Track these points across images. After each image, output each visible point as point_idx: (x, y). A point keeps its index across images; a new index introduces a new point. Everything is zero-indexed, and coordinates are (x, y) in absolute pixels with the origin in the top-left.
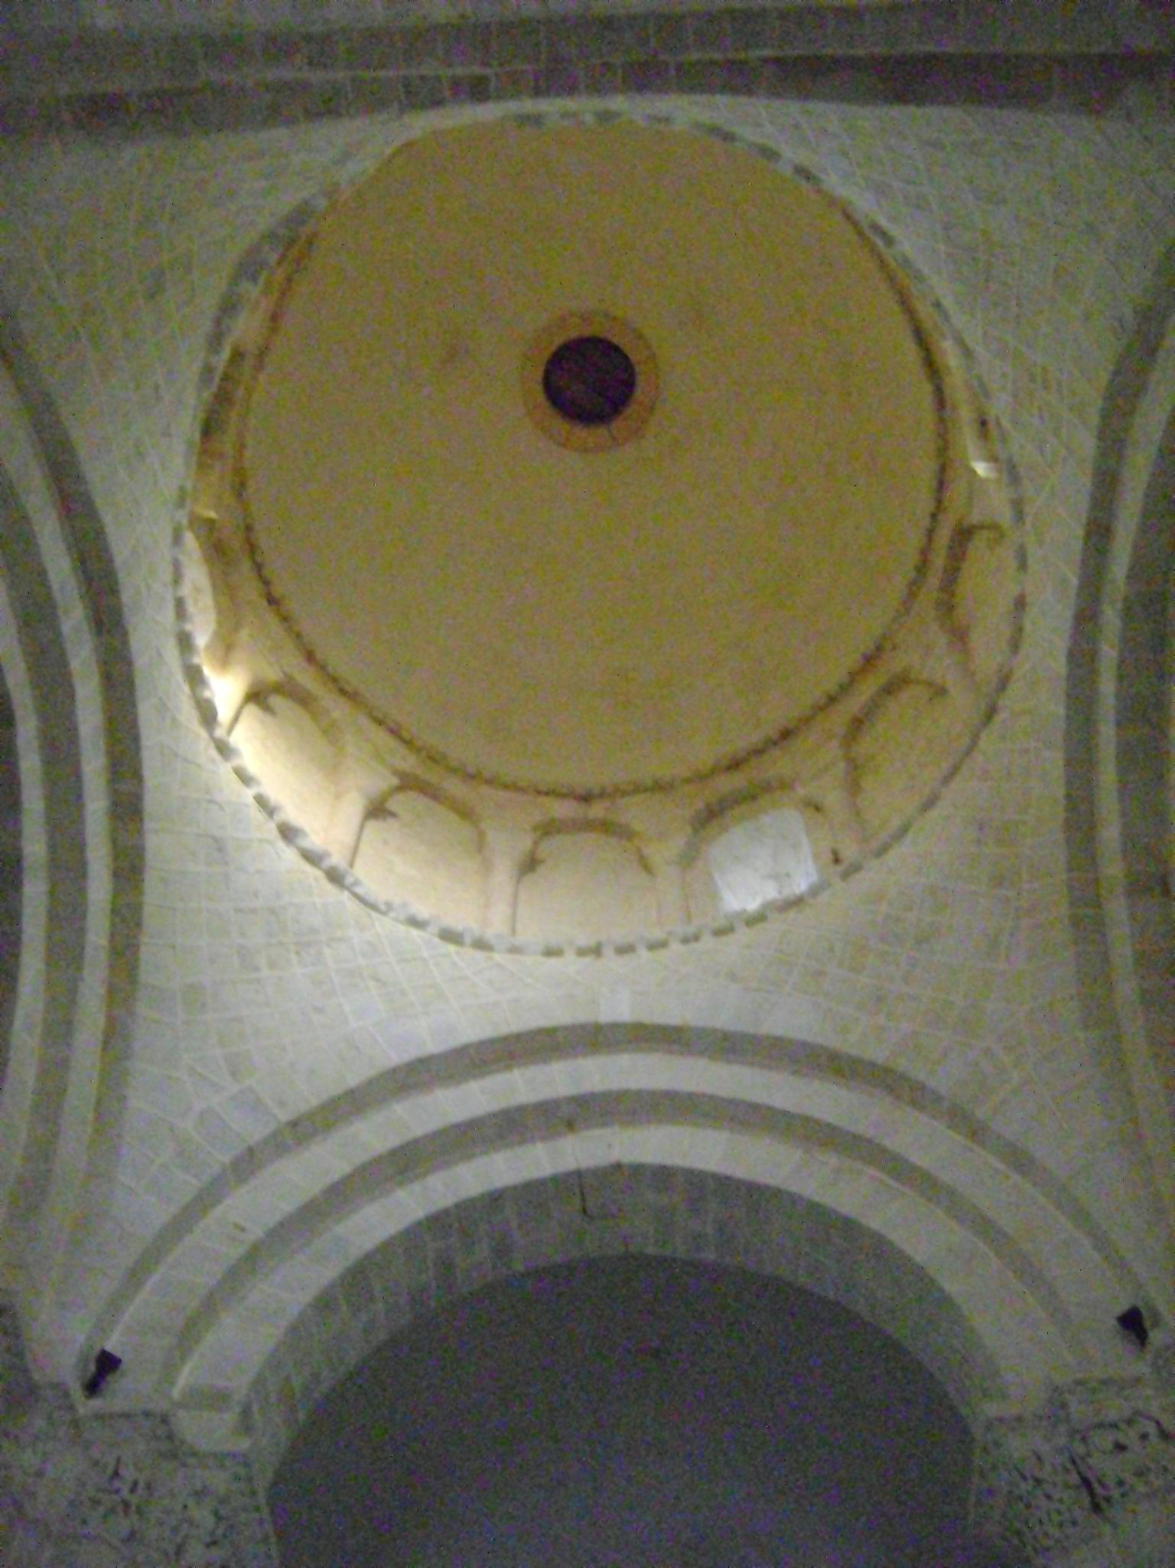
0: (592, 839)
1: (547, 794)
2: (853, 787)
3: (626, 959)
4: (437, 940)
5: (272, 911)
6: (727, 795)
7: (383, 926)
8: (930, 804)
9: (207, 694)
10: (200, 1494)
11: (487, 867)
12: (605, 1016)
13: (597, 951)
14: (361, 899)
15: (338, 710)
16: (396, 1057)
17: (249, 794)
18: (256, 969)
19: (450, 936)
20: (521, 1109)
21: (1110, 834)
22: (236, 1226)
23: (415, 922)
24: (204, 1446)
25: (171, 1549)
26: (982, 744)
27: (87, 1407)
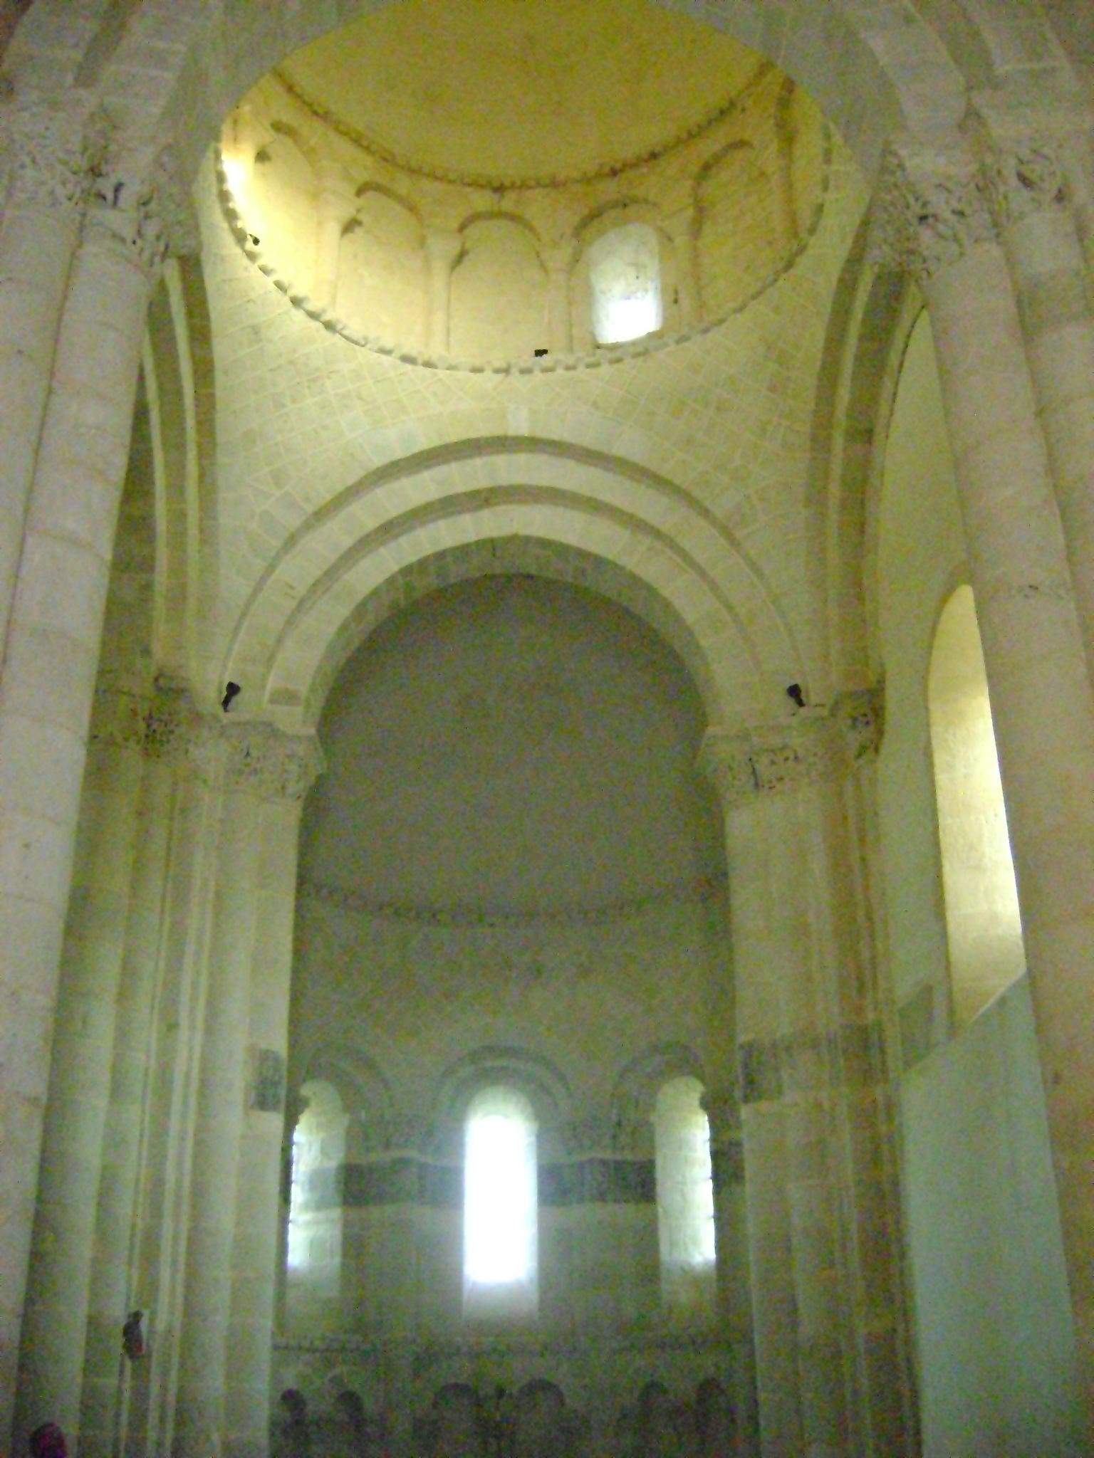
0: (504, 224)
1: (470, 185)
2: (696, 230)
3: (527, 377)
4: (399, 362)
5: (291, 362)
6: (603, 200)
7: (365, 356)
8: (741, 309)
9: (231, 205)
10: (290, 757)
11: (427, 268)
12: (512, 432)
13: (506, 371)
14: (346, 338)
15: (314, 132)
16: (378, 461)
17: (269, 281)
18: (284, 406)
19: (407, 359)
20: (457, 496)
21: (844, 394)
22: (287, 584)
23: (383, 351)
24: (290, 731)
25: (279, 786)
26: (780, 282)
27: (226, 718)
